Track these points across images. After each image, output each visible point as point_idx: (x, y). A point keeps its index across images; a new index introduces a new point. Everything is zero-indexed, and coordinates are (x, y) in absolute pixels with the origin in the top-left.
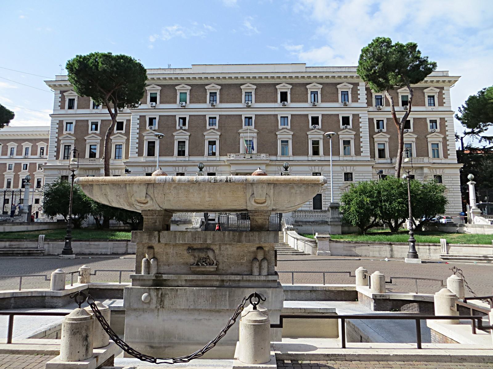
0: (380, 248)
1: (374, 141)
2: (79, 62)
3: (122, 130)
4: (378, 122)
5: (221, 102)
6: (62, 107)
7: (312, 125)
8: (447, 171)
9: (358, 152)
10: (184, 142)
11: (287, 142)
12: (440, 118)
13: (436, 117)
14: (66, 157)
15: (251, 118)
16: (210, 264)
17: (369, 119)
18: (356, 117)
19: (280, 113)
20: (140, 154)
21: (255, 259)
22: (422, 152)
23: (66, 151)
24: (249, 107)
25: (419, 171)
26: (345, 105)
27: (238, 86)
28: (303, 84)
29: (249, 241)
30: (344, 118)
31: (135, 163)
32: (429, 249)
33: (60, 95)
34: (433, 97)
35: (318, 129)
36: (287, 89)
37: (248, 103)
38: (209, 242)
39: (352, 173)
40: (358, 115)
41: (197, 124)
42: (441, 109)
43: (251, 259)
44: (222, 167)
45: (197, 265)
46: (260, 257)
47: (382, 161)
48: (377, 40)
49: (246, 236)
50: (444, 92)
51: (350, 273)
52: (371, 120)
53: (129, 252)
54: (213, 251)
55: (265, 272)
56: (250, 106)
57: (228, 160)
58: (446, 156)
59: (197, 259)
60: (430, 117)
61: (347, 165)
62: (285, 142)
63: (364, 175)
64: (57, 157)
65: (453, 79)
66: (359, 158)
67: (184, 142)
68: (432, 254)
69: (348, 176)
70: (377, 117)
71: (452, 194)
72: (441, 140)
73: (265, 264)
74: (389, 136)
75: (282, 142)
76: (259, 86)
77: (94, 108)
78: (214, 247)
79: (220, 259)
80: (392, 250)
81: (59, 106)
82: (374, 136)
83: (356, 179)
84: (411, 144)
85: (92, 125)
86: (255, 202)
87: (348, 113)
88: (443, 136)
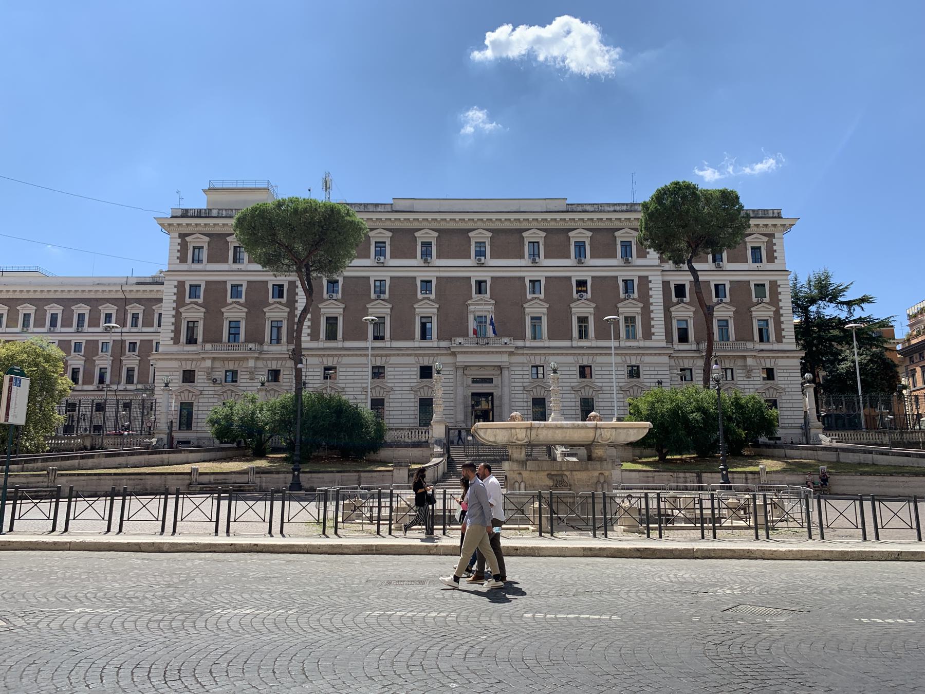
4: (717, 286)
6: (183, 260)
8: (781, 362)
9: (648, 335)
11: (540, 318)
17: (663, 282)
18: (644, 281)
20: (176, 340)
22: (744, 335)
24: (481, 265)
25: (740, 362)
26: (627, 261)
27: (465, 233)
31: (167, 354)
33: (179, 241)
34: (759, 248)
37: (479, 260)
39: (638, 367)
40: (647, 277)
41: (509, 293)
50: (774, 241)
52: (666, 284)
58: (779, 339)
60: (754, 279)
61: (630, 355)
62: (536, 319)
65: (787, 223)
66: (648, 343)
69: (634, 372)
71: (790, 397)
72: (771, 314)
75: (532, 318)
76: (442, 233)
81: (178, 258)
82: (672, 309)
83: (647, 376)
84: (767, 321)
88: (774, 309)
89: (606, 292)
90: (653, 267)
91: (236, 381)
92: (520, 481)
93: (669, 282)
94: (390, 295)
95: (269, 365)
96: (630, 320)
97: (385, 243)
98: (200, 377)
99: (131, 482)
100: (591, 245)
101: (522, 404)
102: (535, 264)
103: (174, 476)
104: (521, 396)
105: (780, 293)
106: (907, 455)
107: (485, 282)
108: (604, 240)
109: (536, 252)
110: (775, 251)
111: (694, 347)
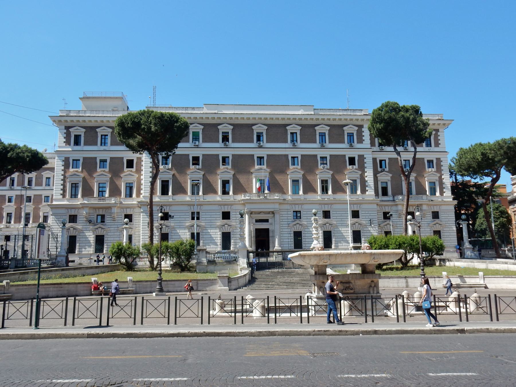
2: (133, 123)
4: (381, 161)
11: (298, 181)
12: (436, 158)
13: (433, 157)
14: (74, 195)
15: (263, 158)
18: (362, 158)
19: (292, 153)
21: (371, 286)
23: (74, 189)
26: (351, 145)
27: (250, 126)
29: (368, 278)
32: (435, 280)
33: (65, 131)
37: (260, 144)
42: (437, 149)
46: (373, 285)
47: (385, 198)
48: (387, 106)
50: (439, 134)
52: (374, 160)
55: (375, 292)
57: (243, 200)
63: (369, 212)
64: (64, 195)
68: (437, 284)
70: (380, 156)
73: (375, 289)
74: (391, 175)
76: (270, 127)
77: (101, 145)
80: (407, 282)
82: (378, 175)
87: (353, 153)
89: (338, 163)
91: (104, 222)
93: (376, 158)
95: (125, 211)
97: (228, 133)
98: (81, 219)
99: (55, 289)
100: (267, 135)
102: (351, 146)
103: (82, 285)
104: (287, 230)
105: (442, 166)
106: (506, 263)
108: (337, 132)
109: (295, 139)
110: (439, 140)
111: (391, 198)
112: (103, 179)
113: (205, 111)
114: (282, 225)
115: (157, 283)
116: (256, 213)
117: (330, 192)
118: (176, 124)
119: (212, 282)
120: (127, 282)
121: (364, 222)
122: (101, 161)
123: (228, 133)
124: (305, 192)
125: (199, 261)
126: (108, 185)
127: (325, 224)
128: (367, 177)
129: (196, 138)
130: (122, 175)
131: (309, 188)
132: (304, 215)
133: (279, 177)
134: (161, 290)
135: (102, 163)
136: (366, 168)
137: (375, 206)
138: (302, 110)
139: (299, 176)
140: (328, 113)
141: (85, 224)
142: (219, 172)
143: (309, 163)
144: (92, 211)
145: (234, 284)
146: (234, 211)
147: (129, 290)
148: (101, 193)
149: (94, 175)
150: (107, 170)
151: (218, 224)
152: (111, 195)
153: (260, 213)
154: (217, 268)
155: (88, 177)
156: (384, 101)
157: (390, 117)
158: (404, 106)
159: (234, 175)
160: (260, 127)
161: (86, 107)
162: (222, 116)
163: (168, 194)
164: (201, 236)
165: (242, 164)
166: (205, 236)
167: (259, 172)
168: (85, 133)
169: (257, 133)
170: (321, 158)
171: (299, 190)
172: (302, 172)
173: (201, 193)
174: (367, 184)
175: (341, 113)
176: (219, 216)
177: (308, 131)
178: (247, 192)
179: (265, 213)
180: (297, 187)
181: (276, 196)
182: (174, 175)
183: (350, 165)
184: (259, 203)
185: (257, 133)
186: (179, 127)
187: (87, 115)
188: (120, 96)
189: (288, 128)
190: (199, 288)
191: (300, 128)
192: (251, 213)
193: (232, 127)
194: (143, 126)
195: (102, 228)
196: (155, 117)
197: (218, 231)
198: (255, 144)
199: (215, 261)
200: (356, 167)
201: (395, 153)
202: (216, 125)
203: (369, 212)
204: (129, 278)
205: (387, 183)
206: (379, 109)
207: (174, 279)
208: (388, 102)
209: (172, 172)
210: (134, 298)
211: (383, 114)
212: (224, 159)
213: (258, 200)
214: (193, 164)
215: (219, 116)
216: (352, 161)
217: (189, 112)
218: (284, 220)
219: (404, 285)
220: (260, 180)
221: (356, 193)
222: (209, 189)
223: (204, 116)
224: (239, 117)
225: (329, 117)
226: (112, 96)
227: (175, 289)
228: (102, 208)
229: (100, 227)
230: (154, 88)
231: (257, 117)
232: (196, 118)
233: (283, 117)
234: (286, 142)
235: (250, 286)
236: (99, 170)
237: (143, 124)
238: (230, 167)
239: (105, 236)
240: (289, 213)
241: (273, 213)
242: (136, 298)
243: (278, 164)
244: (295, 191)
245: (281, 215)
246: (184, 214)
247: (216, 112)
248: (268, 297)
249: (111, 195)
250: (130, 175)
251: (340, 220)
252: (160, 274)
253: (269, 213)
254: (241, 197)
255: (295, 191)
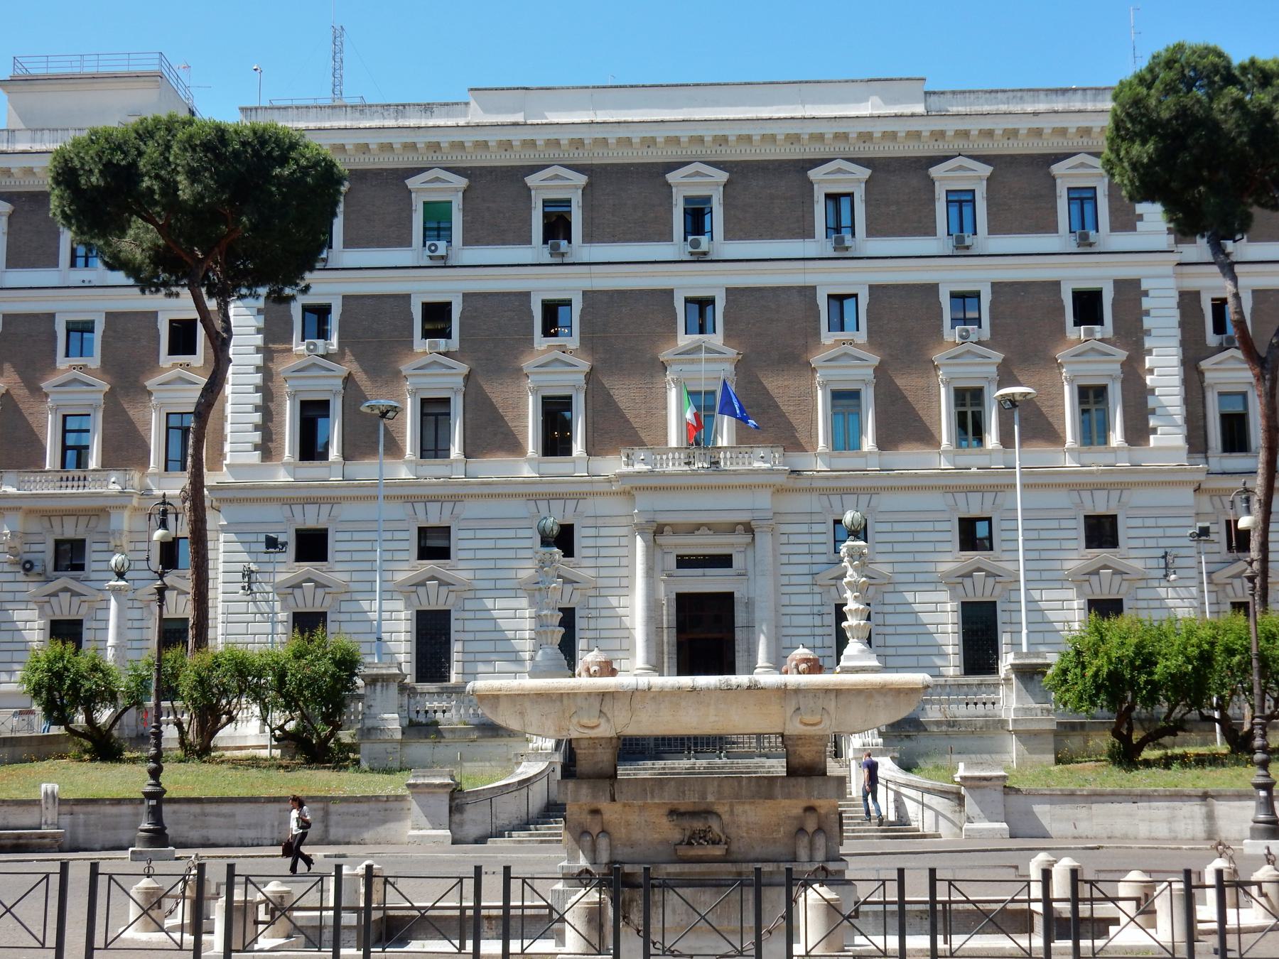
0: (1174, 808)
1: (1202, 382)
2: (109, 169)
3: (193, 352)
5: (993, 230)
7: (953, 327)
10: (446, 401)
11: (855, 395)
15: (711, 301)
16: (714, 843)
18: (1130, 291)
20: (267, 448)
21: (801, 830)
27: (799, 170)
28: (918, 160)
30: (1078, 296)
35: (979, 343)
36: (711, 185)
37: (696, 244)
38: (710, 798)
40: (1137, 282)
43: (794, 830)
44: (599, 501)
45: (690, 844)
46: (811, 826)
48: (1169, 64)
49: (782, 787)
51: (1016, 867)
52: (1189, 300)
53: (332, 838)
54: (719, 816)
56: (705, 253)
57: (622, 476)
59: (688, 833)
63: (1162, 522)
67: (446, 401)
73: (820, 841)
76: (740, 172)
78: (720, 809)
79: (733, 831)
80: (1210, 817)
82: (1204, 364)
85: (68, 332)
86: (801, 722)
87: (1095, 274)
89: (1025, 321)
90: (1149, 252)
91: (81, 567)
92: (596, 830)
94: (462, 340)
95: (421, 515)
96: (1091, 396)
97: (567, 203)
100: (465, 211)
101: (808, 621)
102: (1085, 244)
104: (807, 600)
107: (568, 303)
108: (1022, 186)
109: (845, 221)
112: (77, 399)
113: (477, 115)
114: (785, 580)
115: (144, 809)
116: (677, 529)
117: (992, 439)
118: (277, 171)
119: (388, 808)
120: (34, 803)
121: (1139, 565)
122: (72, 328)
123: (567, 203)
124: (884, 442)
125: (369, 723)
126: (97, 424)
127: (969, 575)
128: (1151, 371)
129: (439, 229)
130: (150, 384)
131: (902, 425)
132: (340, 546)
133: (777, 385)
134: (158, 837)
135: (75, 336)
136: (1148, 333)
137: (1187, 496)
138: (875, 99)
139: (861, 374)
140: (986, 108)
141: (10, 577)
142: (528, 364)
143: (904, 320)
144: (35, 525)
145: (475, 820)
146: (590, 522)
147: (43, 836)
148: (74, 454)
149: (46, 385)
150: (95, 362)
151: (943, 567)
152: (109, 463)
153: (694, 528)
154: (442, 751)
155: (20, 392)
156: (1157, 43)
157: (1182, 113)
158: (1253, 62)
159: (590, 376)
160: (697, 174)
161: (22, 116)
162: (541, 137)
163: (568, 452)
164: (580, 624)
165: (625, 331)
166: (470, 626)
167: (692, 362)
168: (10, 217)
169: (687, 200)
170: (954, 295)
171: (860, 432)
172: (875, 359)
173: (456, 451)
174: (1151, 402)
175: (1041, 107)
176: (1072, 534)
177: (900, 186)
178: (641, 444)
179: (713, 528)
180: (852, 418)
181: (761, 460)
182: (348, 380)
183: (1078, 323)
184: (691, 488)
185: (687, 200)
186: (293, 183)
187: (20, 147)
188: (153, 67)
189: (814, 174)
190: (334, 833)
191: (867, 173)
192: (659, 530)
193: (582, 180)
194: (146, 183)
195: (75, 594)
196: (189, 145)
197: (1072, 593)
198: (676, 248)
199: (436, 723)
200: (1106, 329)
201: (1215, 269)
202: (516, 175)
203: (1162, 522)
204: (46, 787)
205: (1244, 395)
206: (1141, 80)
207: (235, 793)
208: (1180, 48)
209: (342, 369)
210: (56, 867)
211: (1153, 102)
212: (552, 311)
213: (684, 474)
214: (427, 334)
215: (527, 135)
216: (1088, 307)
217: (412, 122)
218: (794, 559)
219: (1199, 829)
220: (691, 394)
221: (1105, 440)
222: (492, 435)
223: (469, 138)
224: (612, 135)
225: (987, 124)
226: (122, 69)
227: (235, 835)
228: (75, 513)
229: (66, 590)
230: (338, 35)
231: (684, 133)
232: (436, 147)
233: (793, 129)
234: (808, 233)
235: (543, 829)
236: (62, 362)
237: (147, 173)
238: (573, 342)
239: (86, 625)
240: (817, 528)
241: (749, 529)
242: (64, 866)
243: (773, 330)
244: (845, 440)
245: (784, 539)
246: (1054, 524)
247: (519, 118)
248: (478, 870)
249: (109, 463)
250: (182, 380)
251: (491, 564)
252: (155, 774)
253: (731, 528)
254: (614, 465)
255: (845, 440)
